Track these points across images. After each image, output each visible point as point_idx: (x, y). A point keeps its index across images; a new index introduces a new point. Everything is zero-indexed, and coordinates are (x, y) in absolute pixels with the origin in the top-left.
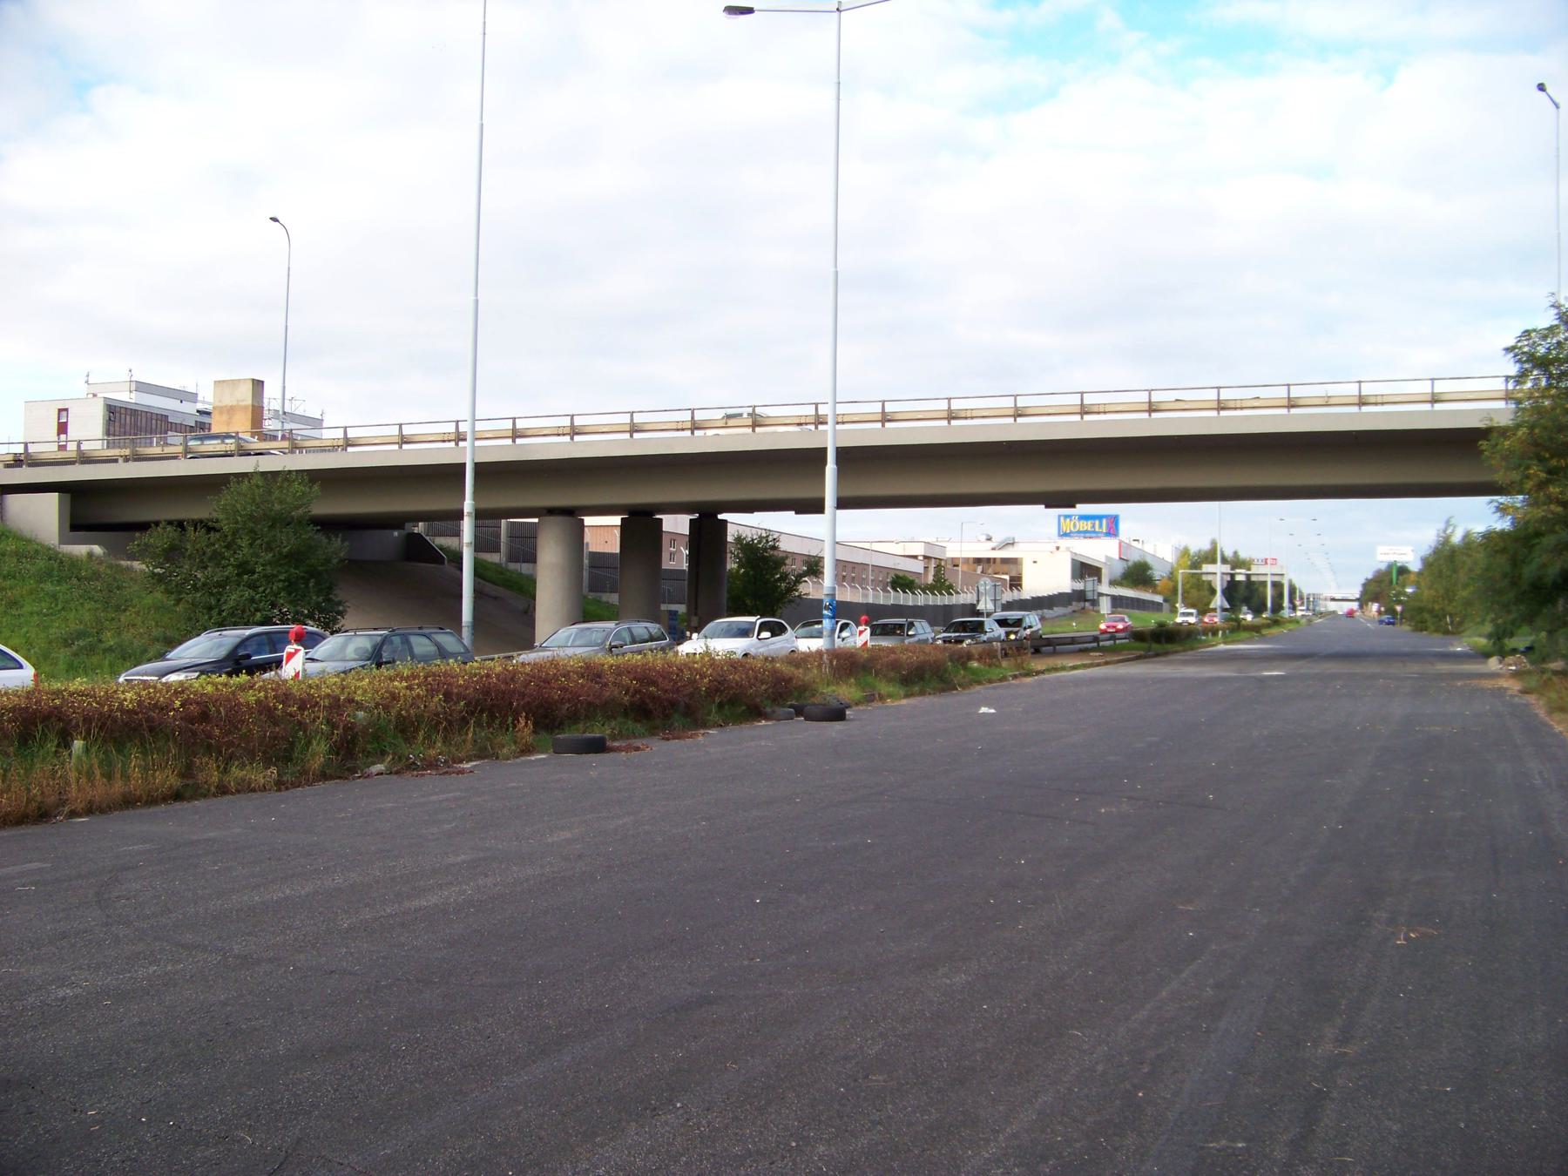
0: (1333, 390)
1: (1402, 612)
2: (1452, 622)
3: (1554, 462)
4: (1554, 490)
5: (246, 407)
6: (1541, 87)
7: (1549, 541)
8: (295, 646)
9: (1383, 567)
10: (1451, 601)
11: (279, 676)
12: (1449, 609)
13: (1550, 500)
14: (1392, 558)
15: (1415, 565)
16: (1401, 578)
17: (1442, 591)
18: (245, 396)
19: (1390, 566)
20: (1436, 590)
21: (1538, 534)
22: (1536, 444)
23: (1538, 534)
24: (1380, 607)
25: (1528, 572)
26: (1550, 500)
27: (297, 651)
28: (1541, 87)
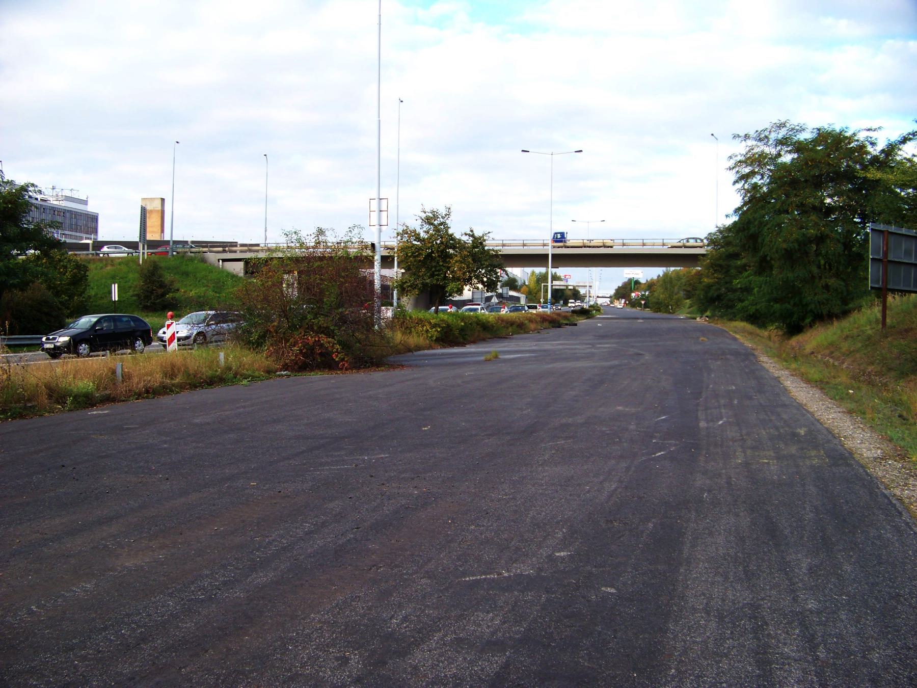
0: (655, 241)
1: (645, 304)
2: (672, 309)
3: (716, 268)
4: (716, 275)
5: (158, 211)
6: (712, 135)
7: (714, 288)
8: (170, 321)
9: (626, 280)
10: (672, 299)
11: (866, 293)
12: (671, 303)
13: (714, 278)
14: (631, 276)
15: (450, 231)
16: (636, 286)
17: (667, 295)
18: (157, 205)
19: (630, 280)
20: (665, 295)
21: (712, 286)
22: (712, 263)
23: (712, 286)
24: (625, 302)
25: (710, 295)
26: (714, 278)
27: (172, 323)
28: (712, 135)
